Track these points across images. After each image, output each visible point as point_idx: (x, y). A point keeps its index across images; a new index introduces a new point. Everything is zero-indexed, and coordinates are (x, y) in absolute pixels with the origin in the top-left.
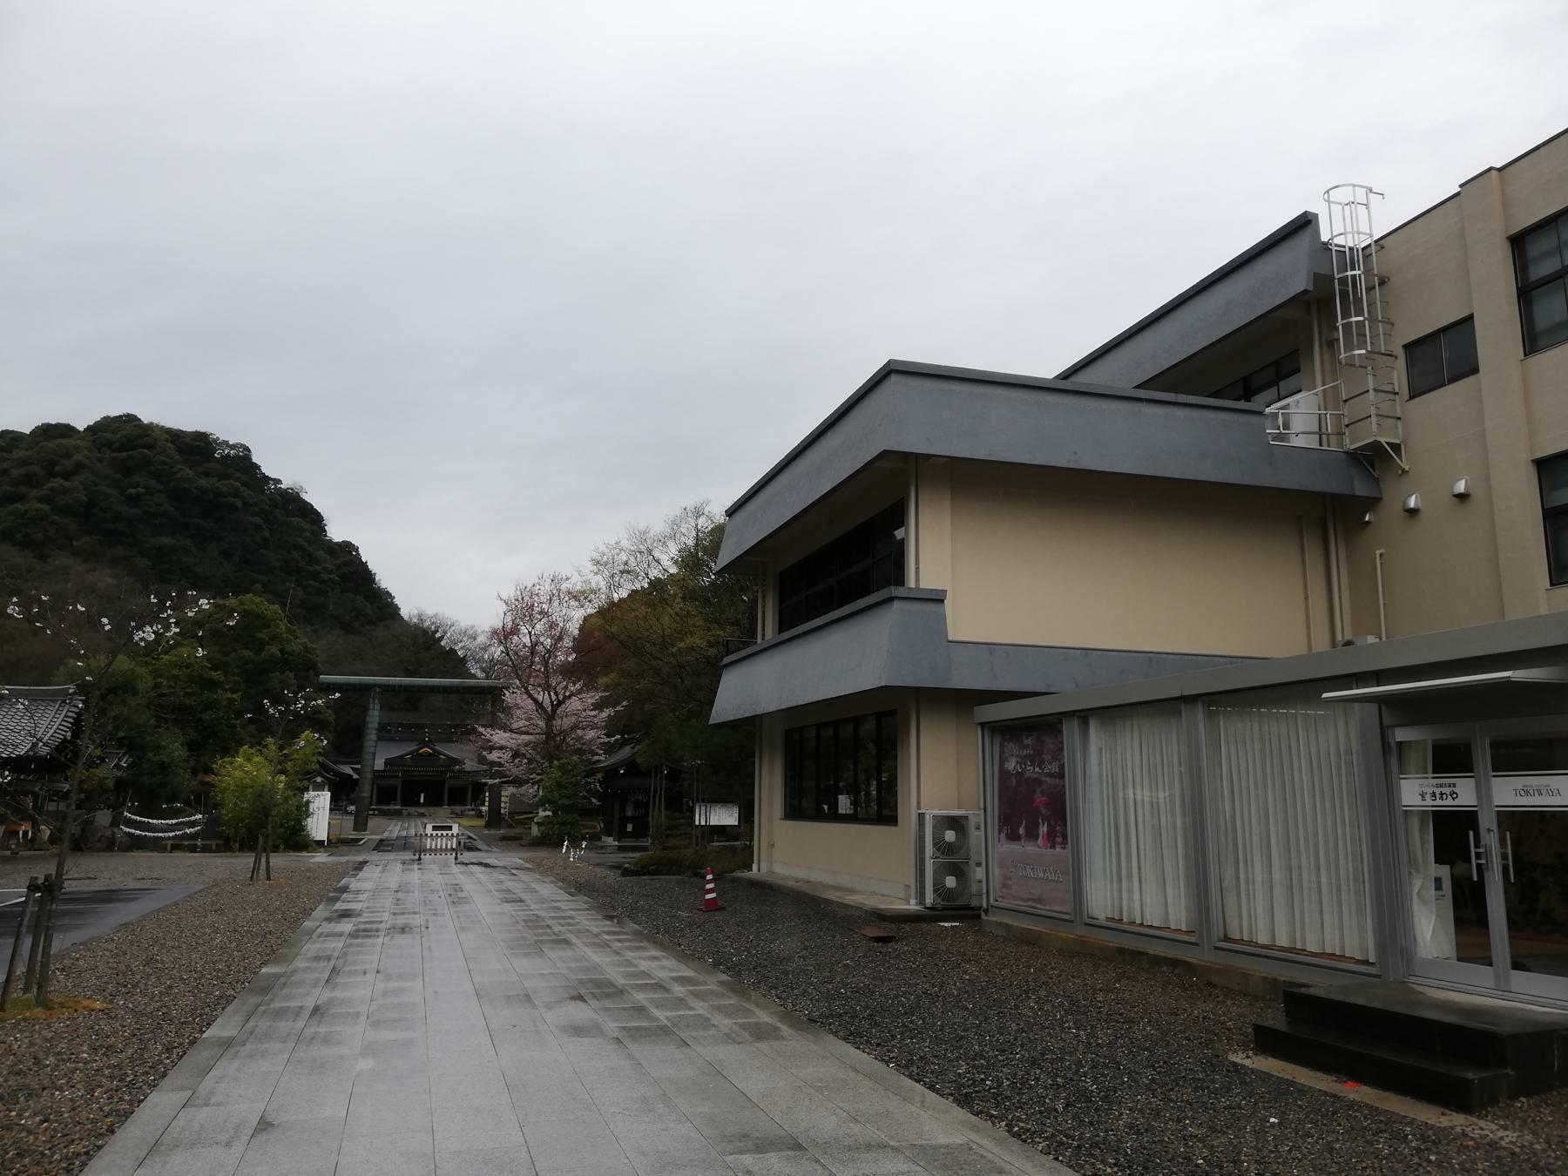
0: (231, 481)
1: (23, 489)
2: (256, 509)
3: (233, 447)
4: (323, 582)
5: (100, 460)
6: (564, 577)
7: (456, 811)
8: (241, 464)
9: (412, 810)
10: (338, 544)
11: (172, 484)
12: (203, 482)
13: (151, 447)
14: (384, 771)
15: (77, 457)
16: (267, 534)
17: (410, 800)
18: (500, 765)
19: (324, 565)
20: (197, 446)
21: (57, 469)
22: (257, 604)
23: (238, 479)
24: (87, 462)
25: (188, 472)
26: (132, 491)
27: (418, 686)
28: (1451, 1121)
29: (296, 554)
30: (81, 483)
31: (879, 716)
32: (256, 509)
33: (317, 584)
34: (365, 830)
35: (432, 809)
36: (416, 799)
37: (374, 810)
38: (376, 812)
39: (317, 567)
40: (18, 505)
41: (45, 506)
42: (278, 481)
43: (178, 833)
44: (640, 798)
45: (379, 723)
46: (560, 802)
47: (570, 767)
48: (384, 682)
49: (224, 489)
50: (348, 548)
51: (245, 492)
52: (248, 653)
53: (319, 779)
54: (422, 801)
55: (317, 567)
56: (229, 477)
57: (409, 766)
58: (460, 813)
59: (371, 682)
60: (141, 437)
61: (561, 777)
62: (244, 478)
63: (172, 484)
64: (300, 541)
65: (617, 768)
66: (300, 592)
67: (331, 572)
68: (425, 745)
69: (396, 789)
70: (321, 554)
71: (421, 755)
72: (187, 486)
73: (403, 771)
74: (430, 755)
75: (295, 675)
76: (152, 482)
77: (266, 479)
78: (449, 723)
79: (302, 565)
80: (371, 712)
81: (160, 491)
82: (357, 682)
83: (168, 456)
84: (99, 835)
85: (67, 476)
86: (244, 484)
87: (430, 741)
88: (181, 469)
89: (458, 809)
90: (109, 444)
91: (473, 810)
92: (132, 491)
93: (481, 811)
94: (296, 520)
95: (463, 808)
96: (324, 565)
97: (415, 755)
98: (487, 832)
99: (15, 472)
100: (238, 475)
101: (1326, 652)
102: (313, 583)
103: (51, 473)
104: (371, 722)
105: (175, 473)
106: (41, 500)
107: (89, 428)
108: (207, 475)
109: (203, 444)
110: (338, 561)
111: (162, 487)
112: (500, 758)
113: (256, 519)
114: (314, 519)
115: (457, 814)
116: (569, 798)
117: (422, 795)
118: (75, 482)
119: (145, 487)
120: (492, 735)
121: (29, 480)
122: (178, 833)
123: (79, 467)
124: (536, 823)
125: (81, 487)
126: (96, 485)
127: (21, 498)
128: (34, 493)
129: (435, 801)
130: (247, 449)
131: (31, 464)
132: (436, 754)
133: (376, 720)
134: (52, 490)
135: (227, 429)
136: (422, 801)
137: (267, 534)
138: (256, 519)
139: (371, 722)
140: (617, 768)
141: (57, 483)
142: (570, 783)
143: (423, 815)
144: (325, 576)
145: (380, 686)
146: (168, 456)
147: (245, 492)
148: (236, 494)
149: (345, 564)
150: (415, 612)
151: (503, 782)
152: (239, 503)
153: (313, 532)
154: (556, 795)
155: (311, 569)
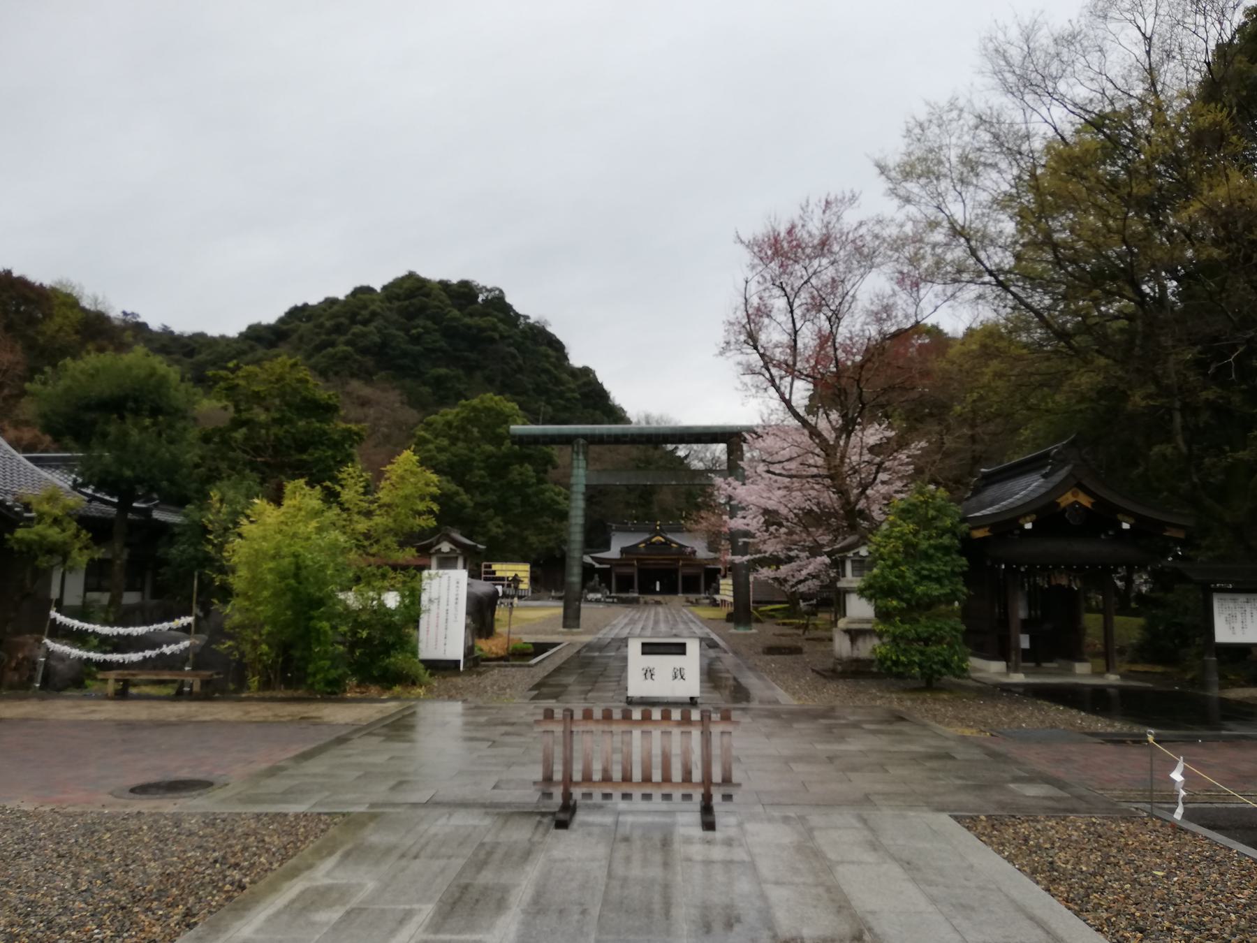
0: (489, 318)
1: (334, 337)
2: (511, 341)
3: (490, 291)
4: (568, 400)
5: (390, 310)
6: (848, 195)
8: (498, 304)
9: (649, 598)
10: (579, 369)
11: (445, 323)
12: (467, 320)
13: (427, 295)
14: (620, 559)
15: (372, 307)
16: (520, 361)
17: (646, 589)
18: (747, 534)
20: (464, 293)
21: (359, 318)
22: (496, 402)
23: (496, 317)
24: (379, 310)
25: (456, 313)
26: (414, 331)
27: (632, 435)
29: (544, 377)
30: (376, 327)
32: (511, 341)
34: (578, 626)
35: (667, 598)
37: (613, 597)
39: (562, 388)
40: (330, 350)
41: (349, 349)
42: (527, 317)
43: (148, 653)
44: (1064, 582)
45: (587, 486)
46: (920, 590)
47: (931, 513)
48: (588, 432)
50: (587, 372)
51: (501, 326)
52: (489, 448)
53: (445, 547)
54: (658, 589)
55: (562, 388)
56: (488, 315)
57: (642, 554)
59: (573, 432)
60: (420, 288)
61: (915, 533)
62: (501, 316)
63: (445, 323)
64: (547, 365)
65: (1019, 518)
66: (550, 409)
67: (573, 391)
68: (658, 534)
70: (565, 377)
71: (654, 543)
72: (455, 324)
73: (638, 560)
74: (662, 543)
76: (429, 324)
77: (518, 316)
78: (674, 483)
79: (550, 386)
80: (575, 472)
81: (435, 330)
82: (556, 432)
83: (440, 301)
84: (20, 656)
85: (365, 323)
86: (501, 320)
88: (450, 311)
89: (692, 597)
90: (398, 298)
91: (707, 598)
92: (414, 331)
93: (715, 600)
94: (543, 348)
95: (697, 596)
97: (648, 543)
98: (733, 631)
99: (328, 324)
100: (496, 313)
101: (734, 585)
103: (353, 321)
104: (577, 484)
105: (446, 314)
106: (347, 343)
107: (385, 288)
108: (471, 315)
109: (466, 290)
111: (436, 327)
112: (748, 525)
113: (512, 350)
114: (557, 347)
115: (692, 602)
116: (938, 580)
117: (658, 584)
118: (371, 328)
119: (423, 328)
120: (735, 489)
121: (338, 329)
122: (148, 653)
123: (374, 314)
124: (847, 631)
125: (375, 330)
126: (386, 328)
127: (333, 344)
128: (342, 339)
129: (670, 589)
130: (501, 291)
131: (338, 317)
132: (668, 543)
133: (583, 481)
134: (354, 334)
135: (485, 278)
136: (658, 589)
137: (520, 361)
138: (512, 350)
139: (577, 484)
140: (1019, 518)
141: (357, 329)
142: (936, 548)
143: (658, 603)
144: (569, 395)
145: (585, 436)
146: (440, 301)
147: (501, 326)
148: (495, 329)
149: (585, 384)
150: (642, 415)
151: (755, 561)
152: (497, 336)
153: (558, 358)
154: (910, 576)
155: (557, 389)
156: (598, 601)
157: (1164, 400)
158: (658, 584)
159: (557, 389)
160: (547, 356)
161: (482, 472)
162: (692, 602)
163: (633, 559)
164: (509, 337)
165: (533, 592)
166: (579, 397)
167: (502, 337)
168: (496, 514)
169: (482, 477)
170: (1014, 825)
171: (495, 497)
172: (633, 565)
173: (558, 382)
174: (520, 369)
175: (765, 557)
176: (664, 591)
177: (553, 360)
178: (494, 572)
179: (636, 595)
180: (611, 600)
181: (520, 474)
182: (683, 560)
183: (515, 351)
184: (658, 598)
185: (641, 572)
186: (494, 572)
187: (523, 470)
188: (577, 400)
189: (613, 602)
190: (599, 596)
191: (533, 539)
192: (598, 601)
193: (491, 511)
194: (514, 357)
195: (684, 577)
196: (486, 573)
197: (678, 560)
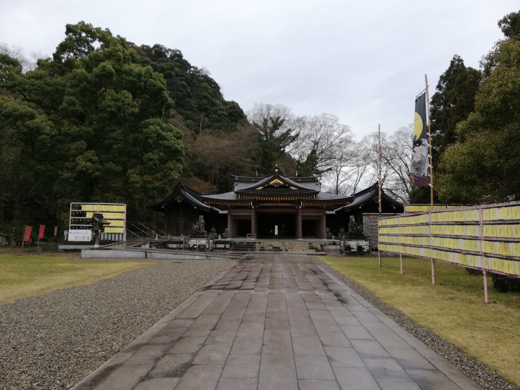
4: (219, 115)
7: (314, 245)
9: (266, 243)
19: (219, 107)
28: (465, 260)
29: (204, 101)
31: (129, 237)
33: (216, 117)
35: (288, 242)
36: (271, 231)
37: (225, 243)
38: (228, 246)
49: (166, 67)
54: (276, 233)
58: (320, 248)
67: (223, 110)
69: (250, 221)
71: (272, 186)
73: (255, 202)
74: (281, 186)
75: (68, 52)
79: (208, 107)
87: (280, 173)
89: (316, 242)
96: (219, 107)
102: (214, 116)
110: (227, 107)
114: (215, 87)
115: (317, 250)
117: (276, 227)
136: (276, 233)
144: (219, 112)
156: (201, 249)
157: (326, 262)
158: (276, 227)
159: (213, 109)
160: (207, 89)
161: (73, 98)
162: (317, 250)
163: (249, 201)
164: (182, 76)
165: (127, 237)
166: (226, 113)
167: (177, 75)
168: (90, 147)
169: (72, 104)
170: (60, 134)
171: (90, 129)
172: (249, 208)
173: (213, 105)
174: (189, 96)
175: (433, 169)
176: (283, 235)
177: (210, 91)
178: (84, 214)
179: (252, 240)
180: (222, 246)
181: (117, 100)
182: (304, 201)
183: (186, 84)
184: (276, 243)
185: (260, 217)
186: (84, 214)
187: (119, 96)
188: (225, 116)
189: (225, 248)
190: (203, 242)
191: (134, 176)
192: (201, 249)
193: (83, 144)
194: (184, 87)
195: (304, 222)
196: (75, 214)
197: (298, 202)
